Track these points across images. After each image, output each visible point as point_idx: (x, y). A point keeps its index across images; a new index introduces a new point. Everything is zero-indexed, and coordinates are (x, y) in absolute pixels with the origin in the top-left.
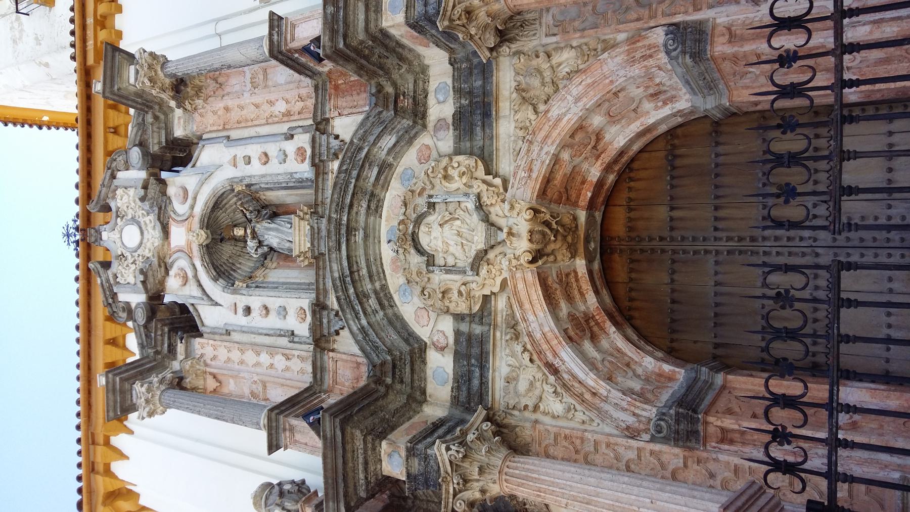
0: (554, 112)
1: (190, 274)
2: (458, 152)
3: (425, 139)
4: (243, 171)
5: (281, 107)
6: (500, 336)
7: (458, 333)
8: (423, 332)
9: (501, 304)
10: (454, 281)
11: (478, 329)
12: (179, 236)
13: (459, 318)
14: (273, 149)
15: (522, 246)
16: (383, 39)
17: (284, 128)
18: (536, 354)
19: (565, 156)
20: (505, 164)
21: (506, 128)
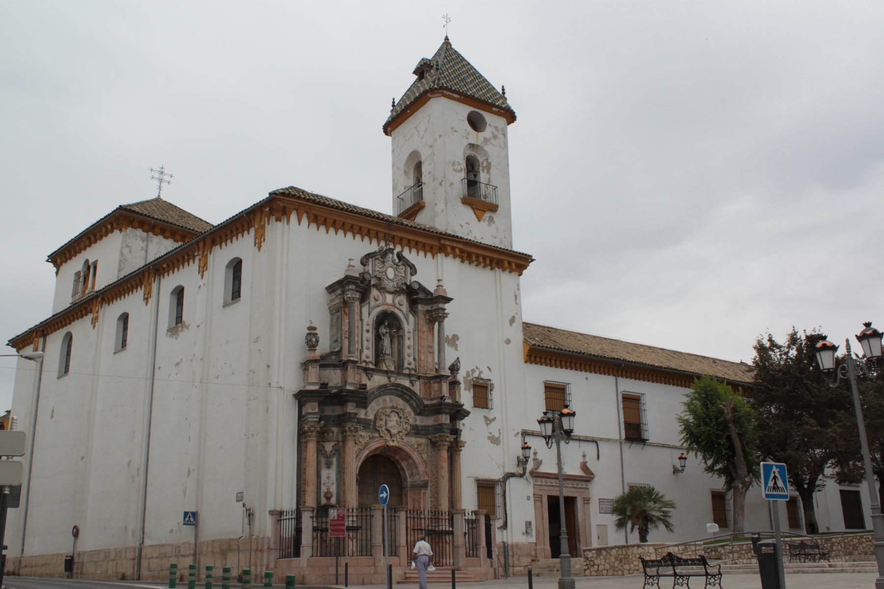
1: (378, 303)
3: (413, 414)
4: (407, 335)
5: (423, 358)
6: (369, 434)
7: (370, 420)
8: (369, 409)
9: (377, 435)
10: (383, 423)
12: (389, 298)
13: (375, 422)
14: (411, 351)
15: (391, 444)
16: (441, 413)
18: (367, 444)
20: (406, 439)
21: (413, 440)
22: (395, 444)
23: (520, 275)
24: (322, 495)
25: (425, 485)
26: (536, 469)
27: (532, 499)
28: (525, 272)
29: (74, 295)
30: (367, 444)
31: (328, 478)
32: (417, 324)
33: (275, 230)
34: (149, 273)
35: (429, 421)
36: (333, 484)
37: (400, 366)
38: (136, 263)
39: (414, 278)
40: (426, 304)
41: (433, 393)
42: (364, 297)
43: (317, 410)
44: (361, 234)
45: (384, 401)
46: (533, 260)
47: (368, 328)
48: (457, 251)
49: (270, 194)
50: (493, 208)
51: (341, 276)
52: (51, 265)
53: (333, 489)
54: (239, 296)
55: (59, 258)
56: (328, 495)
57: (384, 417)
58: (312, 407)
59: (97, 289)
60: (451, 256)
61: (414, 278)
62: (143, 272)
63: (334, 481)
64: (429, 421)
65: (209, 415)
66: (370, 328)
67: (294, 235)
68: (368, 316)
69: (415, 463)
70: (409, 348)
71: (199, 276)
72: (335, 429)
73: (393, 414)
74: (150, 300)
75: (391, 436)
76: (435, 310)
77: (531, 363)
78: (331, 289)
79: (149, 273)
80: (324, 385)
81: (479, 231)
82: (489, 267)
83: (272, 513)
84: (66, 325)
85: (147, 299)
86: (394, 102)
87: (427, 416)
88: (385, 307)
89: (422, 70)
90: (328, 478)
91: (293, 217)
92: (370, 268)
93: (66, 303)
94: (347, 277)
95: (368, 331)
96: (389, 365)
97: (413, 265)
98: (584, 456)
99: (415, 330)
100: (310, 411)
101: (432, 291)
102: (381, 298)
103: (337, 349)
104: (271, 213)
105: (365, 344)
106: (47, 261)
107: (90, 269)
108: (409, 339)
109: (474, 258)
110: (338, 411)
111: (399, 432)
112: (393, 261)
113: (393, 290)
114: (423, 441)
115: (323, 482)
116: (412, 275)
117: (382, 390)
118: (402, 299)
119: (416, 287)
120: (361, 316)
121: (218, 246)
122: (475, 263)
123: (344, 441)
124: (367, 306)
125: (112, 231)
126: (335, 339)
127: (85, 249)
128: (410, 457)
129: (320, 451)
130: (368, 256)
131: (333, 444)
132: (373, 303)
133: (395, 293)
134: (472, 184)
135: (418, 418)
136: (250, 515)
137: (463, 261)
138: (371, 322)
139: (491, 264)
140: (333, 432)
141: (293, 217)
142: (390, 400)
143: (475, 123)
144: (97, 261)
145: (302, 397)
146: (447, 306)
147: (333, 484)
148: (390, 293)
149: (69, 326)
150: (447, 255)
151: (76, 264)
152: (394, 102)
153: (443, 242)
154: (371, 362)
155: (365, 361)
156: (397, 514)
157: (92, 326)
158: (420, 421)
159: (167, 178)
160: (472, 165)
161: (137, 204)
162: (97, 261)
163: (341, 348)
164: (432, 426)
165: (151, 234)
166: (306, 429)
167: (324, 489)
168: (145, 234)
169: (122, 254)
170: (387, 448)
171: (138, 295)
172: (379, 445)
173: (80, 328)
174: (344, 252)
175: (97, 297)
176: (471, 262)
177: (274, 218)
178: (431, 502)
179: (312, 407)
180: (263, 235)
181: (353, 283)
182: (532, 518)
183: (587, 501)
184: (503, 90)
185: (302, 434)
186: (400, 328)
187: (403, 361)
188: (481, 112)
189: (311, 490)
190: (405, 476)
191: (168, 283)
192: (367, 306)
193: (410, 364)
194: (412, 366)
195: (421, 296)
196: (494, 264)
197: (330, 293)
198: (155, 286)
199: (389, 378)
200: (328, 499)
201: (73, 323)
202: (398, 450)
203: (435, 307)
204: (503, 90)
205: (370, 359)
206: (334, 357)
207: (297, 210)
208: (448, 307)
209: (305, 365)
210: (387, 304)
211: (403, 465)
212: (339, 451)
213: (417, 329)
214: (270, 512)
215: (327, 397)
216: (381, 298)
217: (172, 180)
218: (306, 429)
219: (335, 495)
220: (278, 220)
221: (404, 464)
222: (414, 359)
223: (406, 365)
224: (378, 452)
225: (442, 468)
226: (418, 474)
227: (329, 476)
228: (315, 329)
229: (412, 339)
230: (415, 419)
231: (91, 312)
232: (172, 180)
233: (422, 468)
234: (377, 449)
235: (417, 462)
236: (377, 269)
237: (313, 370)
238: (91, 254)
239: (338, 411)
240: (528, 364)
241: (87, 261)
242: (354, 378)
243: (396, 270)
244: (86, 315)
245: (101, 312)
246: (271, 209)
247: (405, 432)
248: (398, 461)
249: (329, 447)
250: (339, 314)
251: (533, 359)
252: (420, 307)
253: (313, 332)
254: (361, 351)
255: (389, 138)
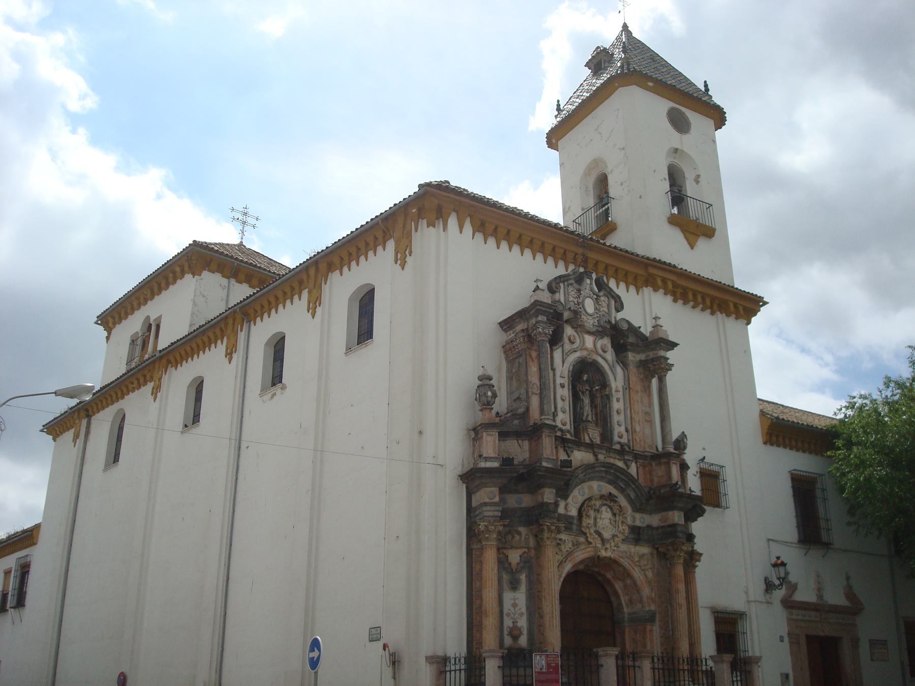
0: (636, 569)
1: (575, 346)
2: (629, 526)
4: (615, 396)
5: (638, 428)
7: (572, 517)
8: (570, 500)
9: (582, 539)
10: (591, 521)
11: (574, 527)
12: (589, 340)
15: (603, 553)
16: (671, 508)
17: (629, 428)
18: (570, 554)
19: (621, 569)
20: (624, 547)
22: (608, 554)
23: (749, 323)
24: (506, 632)
25: (651, 619)
26: (791, 596)
27: (786, 639)
28: (753, 319)
29: (128, 363)
30: (570, 554)
31: (515, 605)
32: (627, 380)
33: (426, 237)
34: (234, 320)
35: (654, 520)
36: (521, 614)
37: (607, 435)
38: (215, 308)
39: (620, 316)
40: (639, 353)
41: (656, 480)
42: (555, 339)
43: (497, 499)
44: (543, 253)
45: (591, 488)
46: (765, 303)
47: (562, 381)
48: (670, 285)
49: (420, 186)
50: (709, 232)
51: (524, 303)
52: (101, 328)
53: (523, 623)
54: (371, 338)
55: (111, 318)
56: (516, 633)
57: (592, 513)
58: (488, 494)
59: (160, 348)
60: (661, 291)
61: (620, 316)
62: (226, 317)
63: (524, 610)
64: (654, 520)
65: (355, 487)
66: (565, 381)
67: (451, 246)
68: (562, 364)
69: (635, 583)
70: (618, 412)
71: (310, 315)
72: (523, 530)
73: (604, 508)
74: (235, 356)
75: (603, 541)
76: (653, 360)
77: (772, 444)
78: (506, 324)
79: (234, 320)
80: (507, 462)
81: (694, 260)
82: (709, 311)
83: (431, 659)
84: (117, 400)
85: (231, 354)
86: (558, 105)
87: (650, 513)
88: (585, 353)
89: (599, 61)
90: (515, 605)
91: (453, 221)
92: (561, 296)
93: (120, 369)
94: (536, 303)
95: (562, 386)
96: (593, 434)
97: (619, 297)
98: (848, 578)
99: (624, 389)
100: (487, 500)
101: (648, 335)
102: (578, 340)
103: (521, 410)
104: (420, 215)
105: (560, 404)
106: (96, 323)
107: (152, 328)
108: (618, 400)
109: (690, 296)
110: (526, 501)
111: (614, 536)
112: (592, 290)
113: (594, 329)
114: (645, 550)
115: (505, 611)
116: (618, 311)
117: (590, 471)
118: (606, 342)
119: (625, 326)
120: (552, 364)
121: (338, 271)
122: (692, 303)
123: (539, 547)
124: (560, 350)
125: (182, 277)
126: (516, 395)
127: (145, 303)
128: (629, 575)
129: (503, 562)
130: (560, 279)
131: (520, 552)
132: (567, 346)
133: (598, 333)
134: (678, 198)
135: (638, 515)
136: (395, 661)
137: (675, 301)
138: (566, 374)
139: (711, 308)
140: (519, 533)
141: (453, 221)
142: (598, 487)
143: (679, 123)
144: (160, 317)
145: (471, 478)
146: (669, 354)
147: (521, 614)
148: (589, 333)
149: (121, 401)
150: (656, 290)
151: (133, 325)
152: (558, 105)
153: (652, 270)
154: (568, 432)
155: (561, 430)
156: (637, 664)
157: (152, 398)
158: (641, 520)
159: (251, 221)
160: (675, 178)
161: (215, 244)
162: (160, 317)
163: (528, 409)
164: (657, 528)
165: (233, 281)
166: (482, 528)
167: (508, 623)
168: (225, 281)
169: (195, 304)
170: (596, 560)
171: (218, 351)
172: (586, 555)
173: (138, 405)
174: (520, 276)
175: (161, 358)
176: (686, 303)
177: (425, 221)
178: (662, 644)
179: (488, 494)
180: (409, 246)
181: (543, 313)
182: (788, 669)
183: (855, 642)
184: (706, 85)
185: (473, 534)
186: (605, 385)
187: (612, 432)
188: (683, 109)
189: (490, 622)
190: (620, 604)
191: (261, 332)
192: (560, 350)
193: (621, 437)
194: (624, 440)
195: (631, 339)
196: (715, 307)
197: (505, 331)
198: (242, 336)
199: (596, 456)
200: (515, 638)
201: (126, 397)
202: (612, 563)
203: (651, 354)
204: (706, 85)
205: (568, 427)
206: (516, 422)
207: (457, 212)
208: (672, 356)
209: (476, 432)
210: (586, 349)
211: (617, 586)
212: (532, 565)
213: (628, 387)
214: (427, 658)
215: (518, 477)
216: (578, 340)
217: (258, 223)
218: (482, 528)
219: (525, 632)
220: (431, 224)
221: (618, 586)
222: (627, 431)
223: (616, 439)
224: (581, 567)
225: (677, 591)
226: (641, 601)
227: (517, 601)
228: (490, 379)
229: (621, 401)
230: (634, 519)
231: (152, 379)
232: (258, 223)
233: (646, 592)
234: (582, 562)
235: (639, 583)
236: (571, 299)
237: (489, 438)
238: (151, 310)
239: (526, 501)
240: (768, 447)
241: (148, 318)
242: (549, 450)
243: (597, 301)
244: (145, 384)
245: (165, 378)
246: (420, 210)
247: (621, 537)
248: (608, 581)
249: (514, 557)
250: (521, 360)
251: (774, 439)
252: (632, 357)
253: (487, 382)
254: (555, 415)
255: (554, 154)
